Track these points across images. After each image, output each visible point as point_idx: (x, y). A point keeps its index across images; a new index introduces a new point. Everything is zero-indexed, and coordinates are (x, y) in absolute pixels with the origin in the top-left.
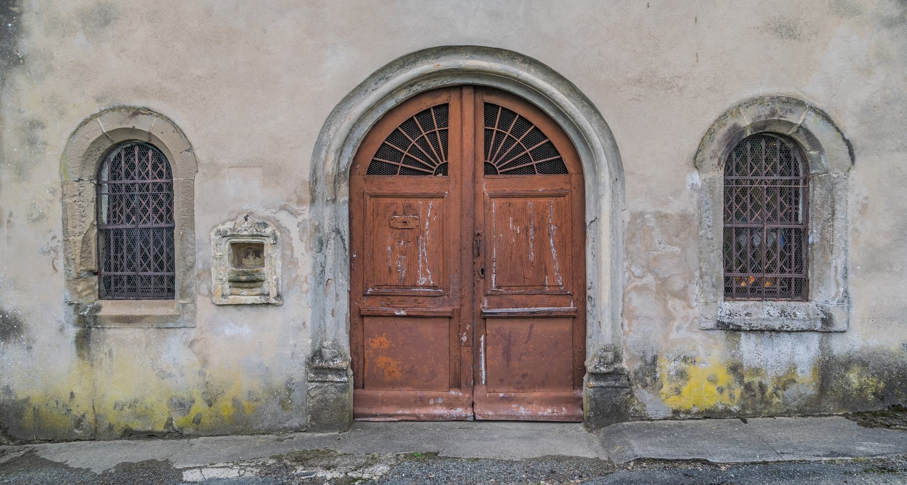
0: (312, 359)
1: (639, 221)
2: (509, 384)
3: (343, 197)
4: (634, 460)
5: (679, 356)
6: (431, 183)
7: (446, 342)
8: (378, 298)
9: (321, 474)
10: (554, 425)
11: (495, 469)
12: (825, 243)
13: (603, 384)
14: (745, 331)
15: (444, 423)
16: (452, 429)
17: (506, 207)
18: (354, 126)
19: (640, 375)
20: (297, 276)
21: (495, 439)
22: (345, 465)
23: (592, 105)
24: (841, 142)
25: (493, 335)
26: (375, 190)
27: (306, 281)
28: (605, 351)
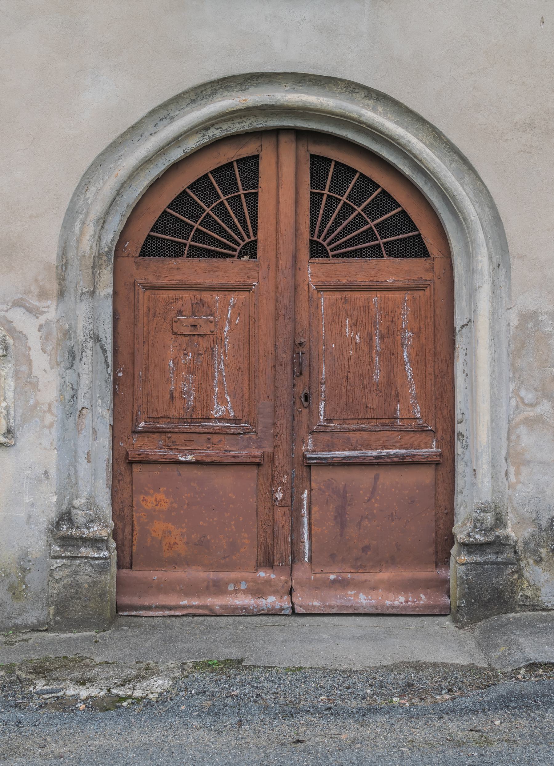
0: (58, 525)
1: (530, 325)
2: (343, 561)
3: (106, 290)
4: (526, 666)
6: (231, 270)
7: (252, 501)
8: (154, 436)
9: (71, 691)
10: (409, 619)
11: (326, 682)
13: (479, 559)
15: (249, 619)
16: (260, 626)
17: (345, 303)
18: (122, 186)
19: (532, 545)
20: (37, 403)
21: (324, 641)
22: (108, 679)
23: (464, 159)
25: (320, 489)
26: (152, 279)
27: (50, 410)
28: (483, 511)
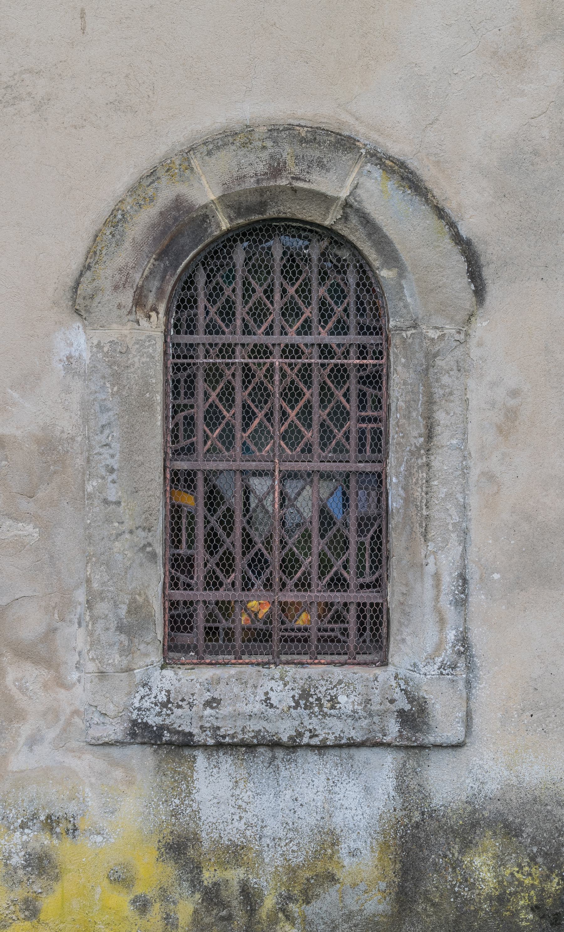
5: (35, 816)
12: (412, 511)
14: (205, 746)
24: (448, 244)
